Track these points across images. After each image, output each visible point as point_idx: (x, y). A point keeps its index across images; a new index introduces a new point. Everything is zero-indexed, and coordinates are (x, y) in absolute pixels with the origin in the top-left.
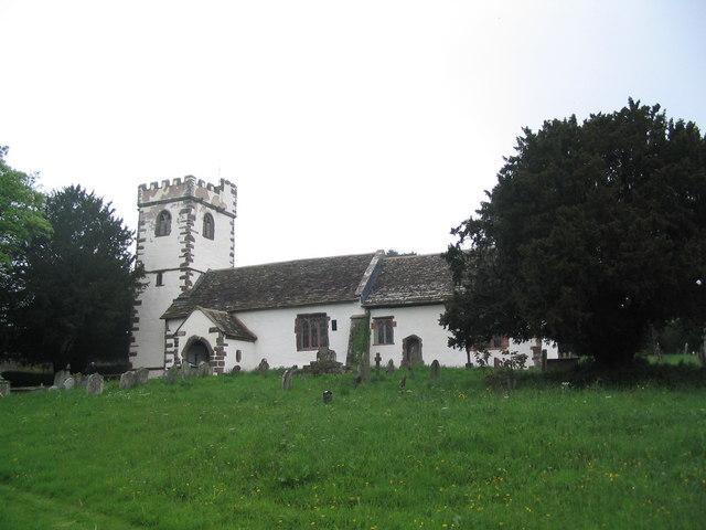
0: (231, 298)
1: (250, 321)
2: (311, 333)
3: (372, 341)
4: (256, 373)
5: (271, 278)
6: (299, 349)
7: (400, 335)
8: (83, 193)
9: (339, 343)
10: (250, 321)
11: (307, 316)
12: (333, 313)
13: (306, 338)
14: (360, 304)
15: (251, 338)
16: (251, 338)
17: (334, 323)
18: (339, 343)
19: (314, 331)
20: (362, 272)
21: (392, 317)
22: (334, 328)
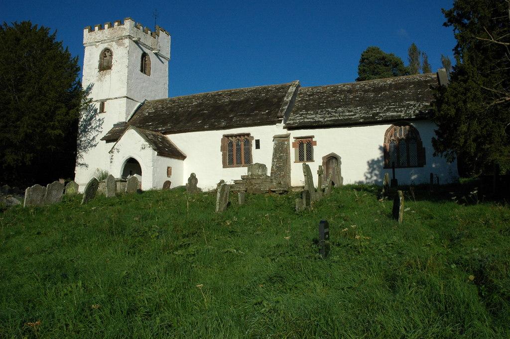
0: (164, 123)
1: (177, 140)
2: (236, 152)
3: (219, 195)
4: (399, 142)
5: (200, 105)
6: (224, 167)
7: (319, 154)
8: (35, 27)
9: (263, 156)
10: (177, 140)
11: (232, 136)
12: (256, 132)
13: (231, 156)
14: (283, 124)
15: (180, 156)
16: (180, 156)
17: (258, 142)
18: (263, 156)
19: (239, 150)
20: (281, 99)
21: (312, 137)
22: (258, 147)
